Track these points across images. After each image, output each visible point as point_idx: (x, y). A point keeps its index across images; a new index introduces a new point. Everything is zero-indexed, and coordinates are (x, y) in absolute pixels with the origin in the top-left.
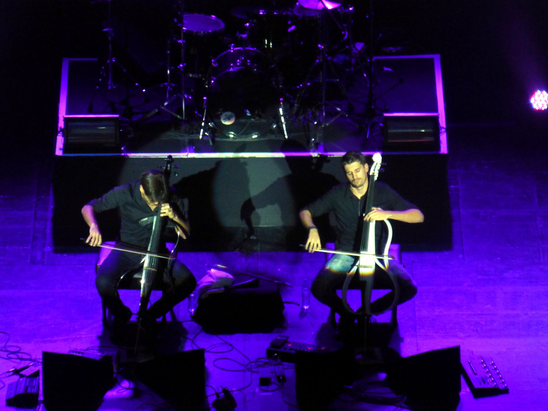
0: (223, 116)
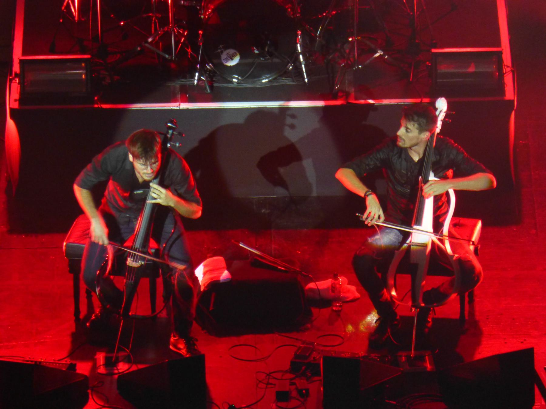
0: (224, 56)
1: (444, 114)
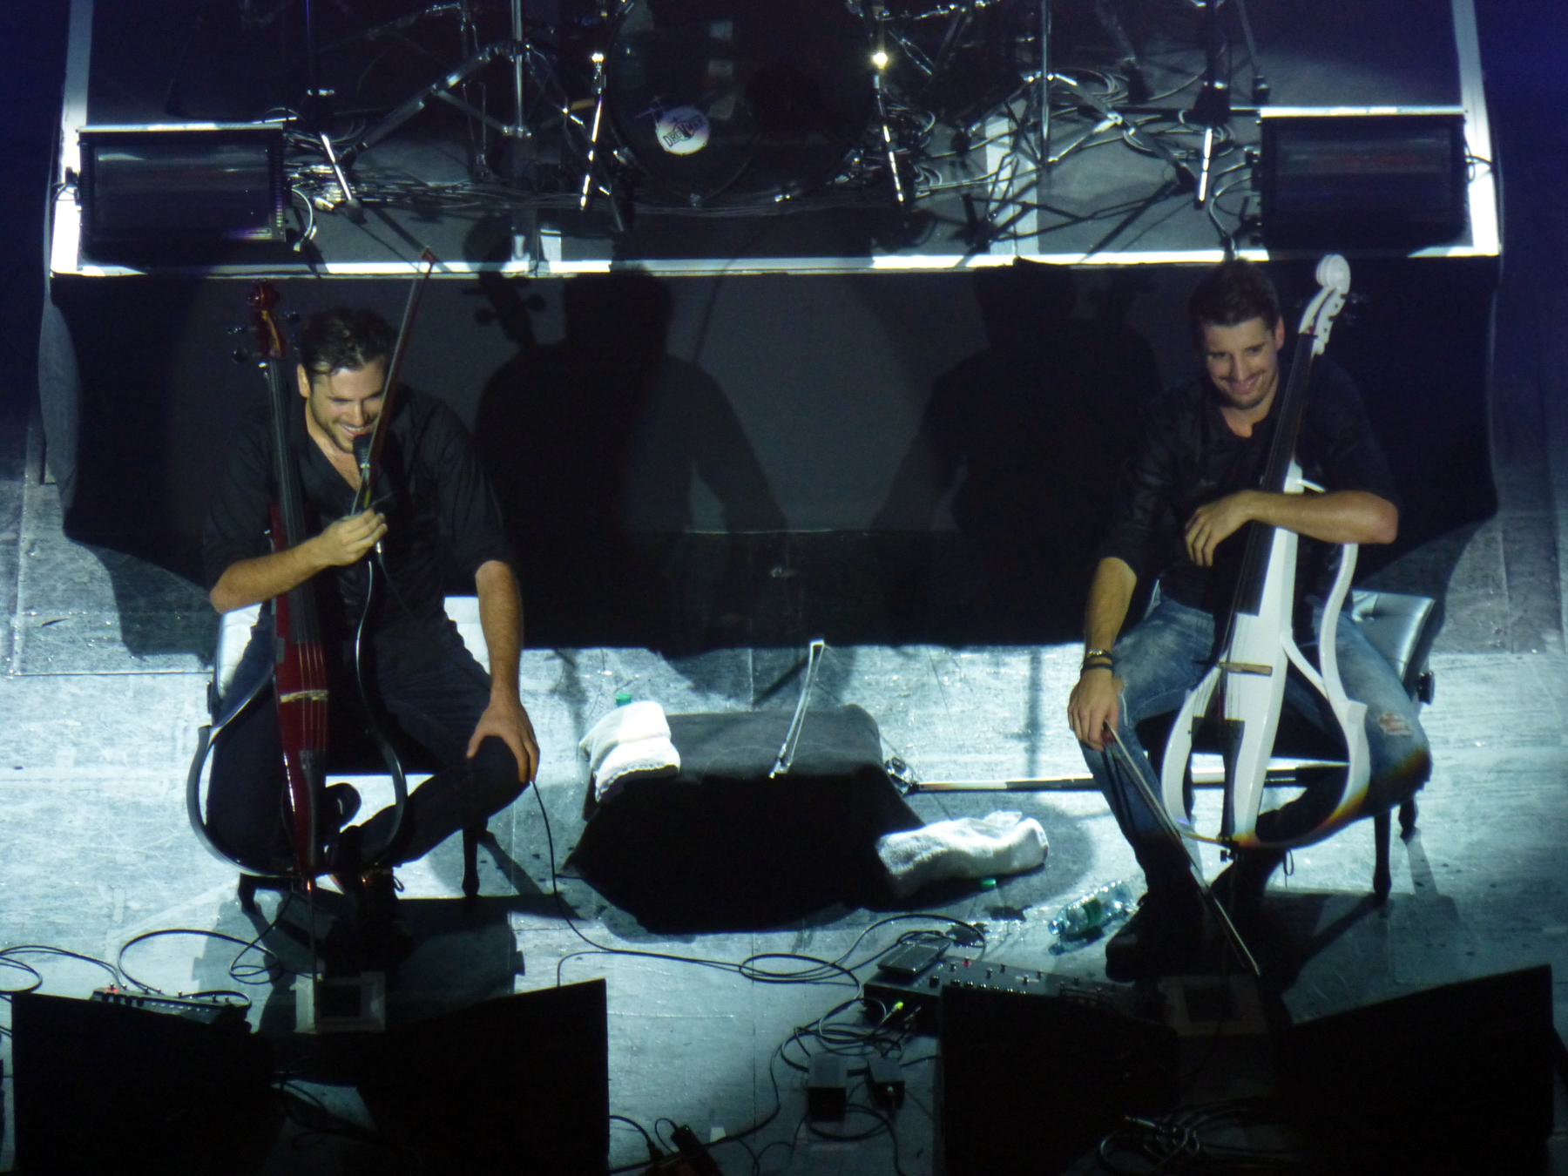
1: (1341, 303)
